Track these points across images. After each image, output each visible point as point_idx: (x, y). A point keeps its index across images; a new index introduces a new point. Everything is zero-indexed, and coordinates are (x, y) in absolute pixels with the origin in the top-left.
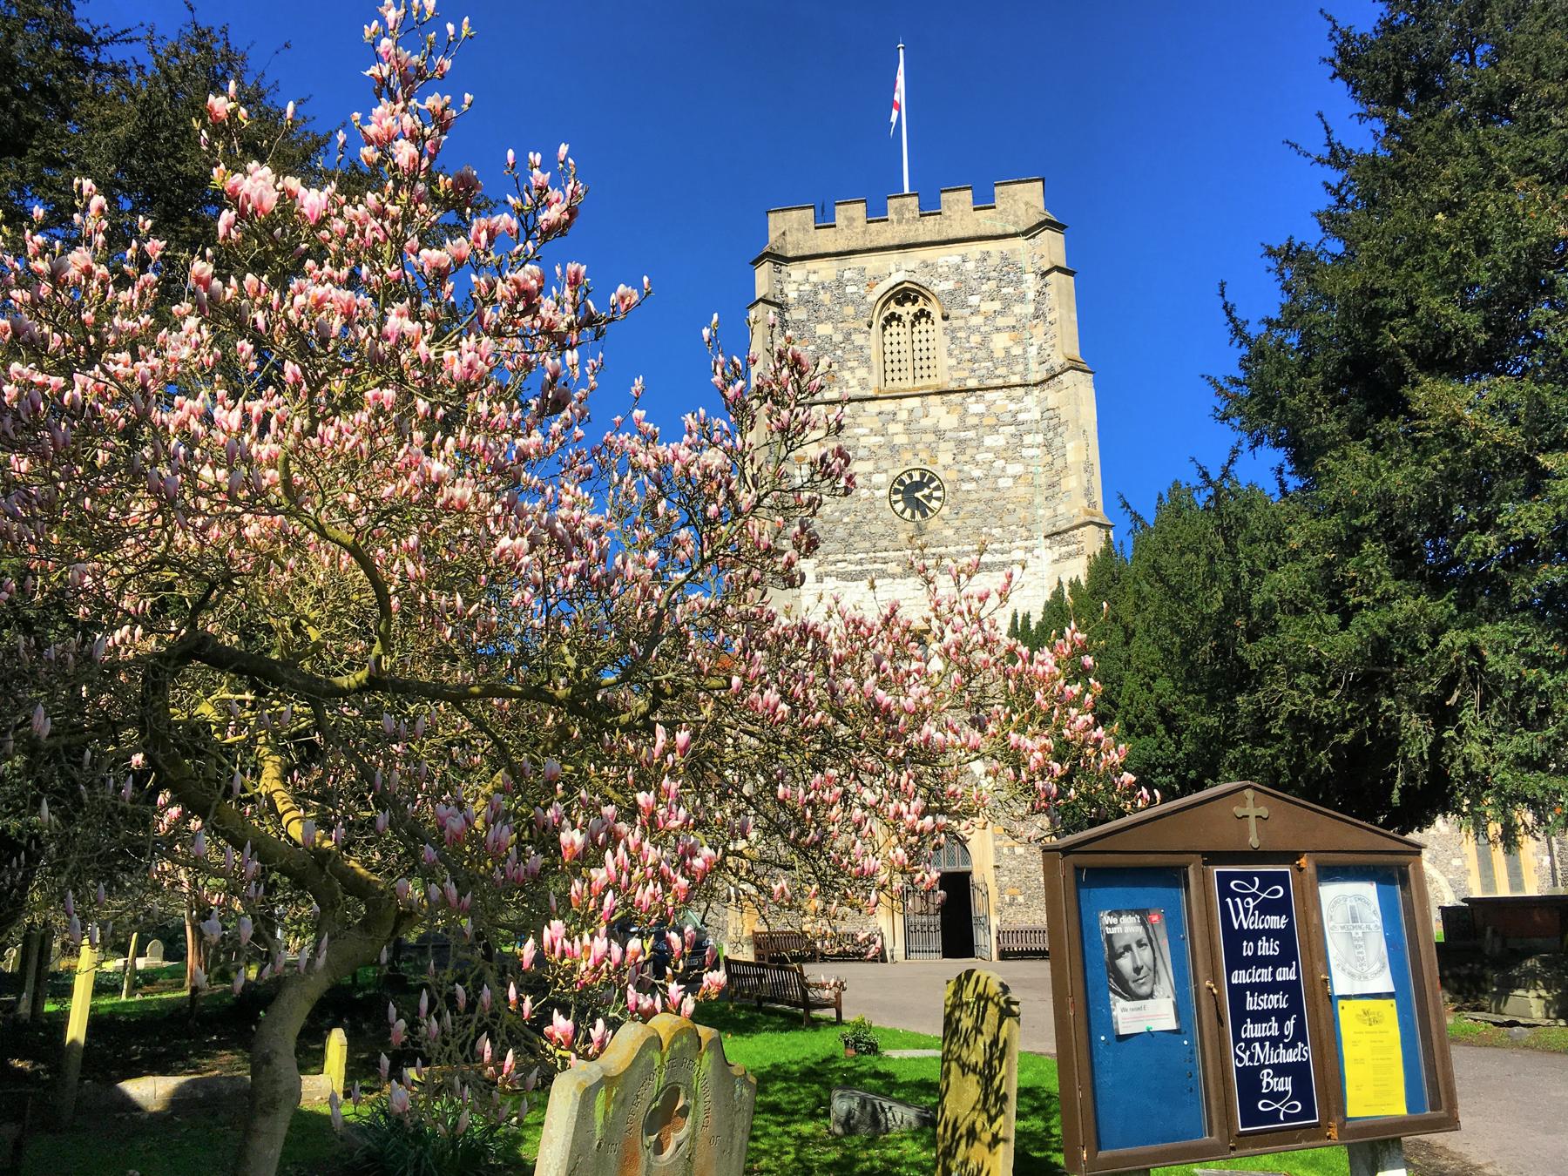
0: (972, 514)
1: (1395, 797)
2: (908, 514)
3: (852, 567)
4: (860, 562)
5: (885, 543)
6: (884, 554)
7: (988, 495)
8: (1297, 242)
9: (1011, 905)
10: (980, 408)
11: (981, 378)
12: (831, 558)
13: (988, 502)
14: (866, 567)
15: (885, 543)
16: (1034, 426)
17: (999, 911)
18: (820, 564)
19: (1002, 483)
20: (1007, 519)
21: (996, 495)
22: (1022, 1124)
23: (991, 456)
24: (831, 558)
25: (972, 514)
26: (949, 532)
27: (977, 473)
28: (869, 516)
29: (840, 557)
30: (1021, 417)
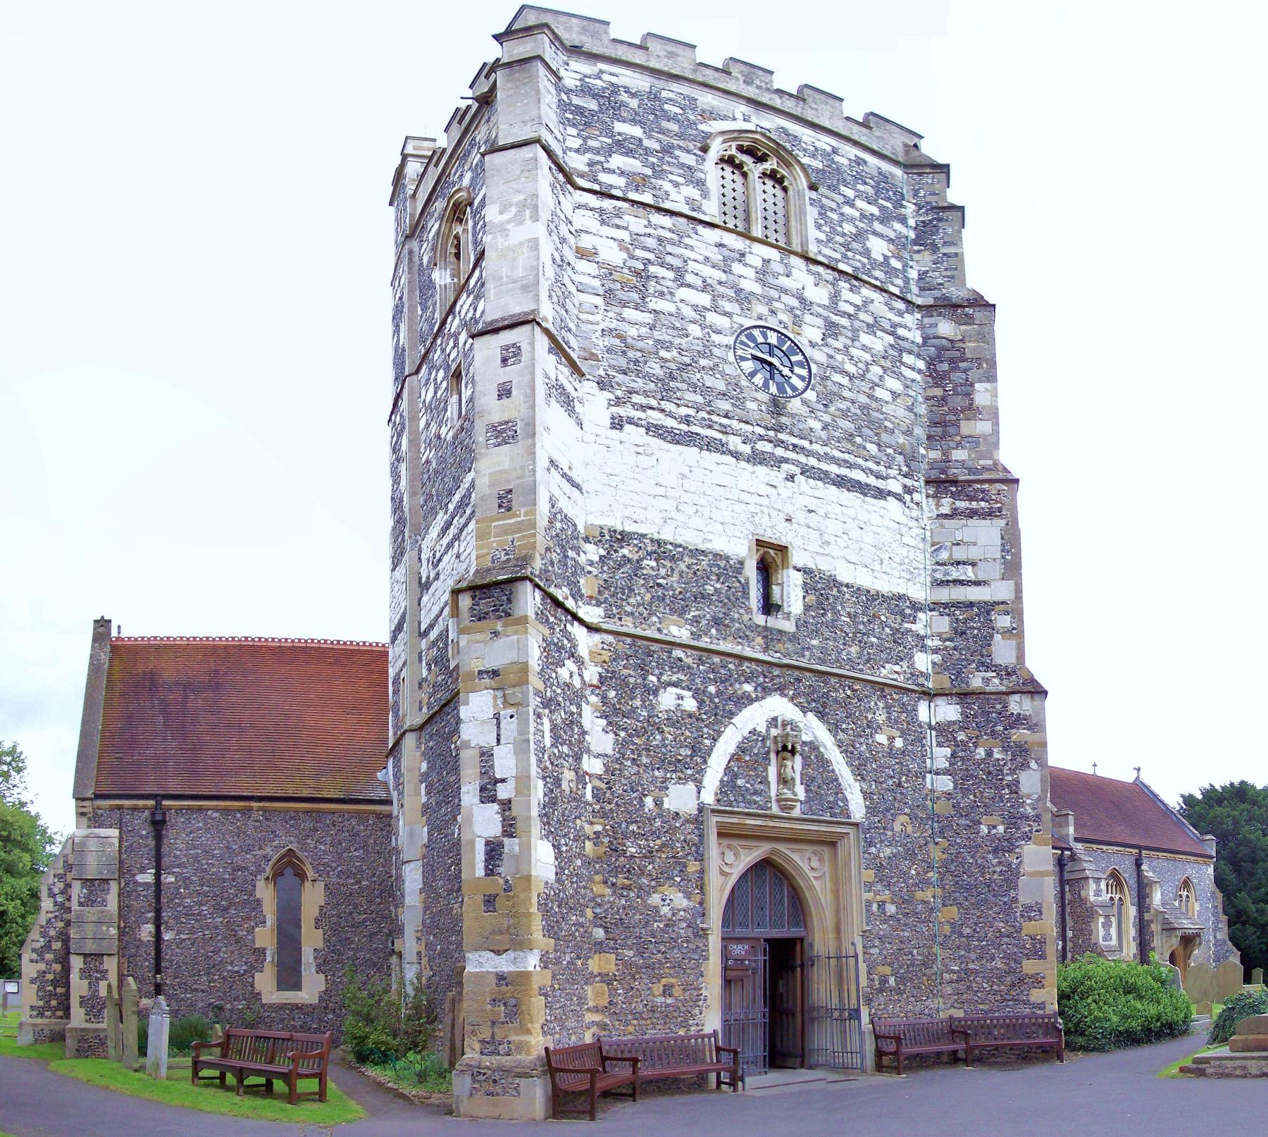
0: (845, 414)
1: (857, 807)
2: (759, 379)
3: (670, 423)
4: (687, 420)
5: (725, 405)
6: (725, 421)
7: (863, 399)
8: (18, 750)
9: (881, 990)
10: (857, 300)
11: (856, 269)
12: (637, 399)
13: (864, 408)
14: (695, 429)
15: (725, 405)
16: (916, 349)
17: (869, 1001)
18: (618, 402)
19: (879, 393)
20: (885, 437)
21: (874, 405)
22: (172, 1060)
23: (868, 357)
24: (637, 399)
25: (845, 414)
26: (817, 426)
27: (850, 368)
28: (703, 362)
29: (654, 403)
30: (901, 331)
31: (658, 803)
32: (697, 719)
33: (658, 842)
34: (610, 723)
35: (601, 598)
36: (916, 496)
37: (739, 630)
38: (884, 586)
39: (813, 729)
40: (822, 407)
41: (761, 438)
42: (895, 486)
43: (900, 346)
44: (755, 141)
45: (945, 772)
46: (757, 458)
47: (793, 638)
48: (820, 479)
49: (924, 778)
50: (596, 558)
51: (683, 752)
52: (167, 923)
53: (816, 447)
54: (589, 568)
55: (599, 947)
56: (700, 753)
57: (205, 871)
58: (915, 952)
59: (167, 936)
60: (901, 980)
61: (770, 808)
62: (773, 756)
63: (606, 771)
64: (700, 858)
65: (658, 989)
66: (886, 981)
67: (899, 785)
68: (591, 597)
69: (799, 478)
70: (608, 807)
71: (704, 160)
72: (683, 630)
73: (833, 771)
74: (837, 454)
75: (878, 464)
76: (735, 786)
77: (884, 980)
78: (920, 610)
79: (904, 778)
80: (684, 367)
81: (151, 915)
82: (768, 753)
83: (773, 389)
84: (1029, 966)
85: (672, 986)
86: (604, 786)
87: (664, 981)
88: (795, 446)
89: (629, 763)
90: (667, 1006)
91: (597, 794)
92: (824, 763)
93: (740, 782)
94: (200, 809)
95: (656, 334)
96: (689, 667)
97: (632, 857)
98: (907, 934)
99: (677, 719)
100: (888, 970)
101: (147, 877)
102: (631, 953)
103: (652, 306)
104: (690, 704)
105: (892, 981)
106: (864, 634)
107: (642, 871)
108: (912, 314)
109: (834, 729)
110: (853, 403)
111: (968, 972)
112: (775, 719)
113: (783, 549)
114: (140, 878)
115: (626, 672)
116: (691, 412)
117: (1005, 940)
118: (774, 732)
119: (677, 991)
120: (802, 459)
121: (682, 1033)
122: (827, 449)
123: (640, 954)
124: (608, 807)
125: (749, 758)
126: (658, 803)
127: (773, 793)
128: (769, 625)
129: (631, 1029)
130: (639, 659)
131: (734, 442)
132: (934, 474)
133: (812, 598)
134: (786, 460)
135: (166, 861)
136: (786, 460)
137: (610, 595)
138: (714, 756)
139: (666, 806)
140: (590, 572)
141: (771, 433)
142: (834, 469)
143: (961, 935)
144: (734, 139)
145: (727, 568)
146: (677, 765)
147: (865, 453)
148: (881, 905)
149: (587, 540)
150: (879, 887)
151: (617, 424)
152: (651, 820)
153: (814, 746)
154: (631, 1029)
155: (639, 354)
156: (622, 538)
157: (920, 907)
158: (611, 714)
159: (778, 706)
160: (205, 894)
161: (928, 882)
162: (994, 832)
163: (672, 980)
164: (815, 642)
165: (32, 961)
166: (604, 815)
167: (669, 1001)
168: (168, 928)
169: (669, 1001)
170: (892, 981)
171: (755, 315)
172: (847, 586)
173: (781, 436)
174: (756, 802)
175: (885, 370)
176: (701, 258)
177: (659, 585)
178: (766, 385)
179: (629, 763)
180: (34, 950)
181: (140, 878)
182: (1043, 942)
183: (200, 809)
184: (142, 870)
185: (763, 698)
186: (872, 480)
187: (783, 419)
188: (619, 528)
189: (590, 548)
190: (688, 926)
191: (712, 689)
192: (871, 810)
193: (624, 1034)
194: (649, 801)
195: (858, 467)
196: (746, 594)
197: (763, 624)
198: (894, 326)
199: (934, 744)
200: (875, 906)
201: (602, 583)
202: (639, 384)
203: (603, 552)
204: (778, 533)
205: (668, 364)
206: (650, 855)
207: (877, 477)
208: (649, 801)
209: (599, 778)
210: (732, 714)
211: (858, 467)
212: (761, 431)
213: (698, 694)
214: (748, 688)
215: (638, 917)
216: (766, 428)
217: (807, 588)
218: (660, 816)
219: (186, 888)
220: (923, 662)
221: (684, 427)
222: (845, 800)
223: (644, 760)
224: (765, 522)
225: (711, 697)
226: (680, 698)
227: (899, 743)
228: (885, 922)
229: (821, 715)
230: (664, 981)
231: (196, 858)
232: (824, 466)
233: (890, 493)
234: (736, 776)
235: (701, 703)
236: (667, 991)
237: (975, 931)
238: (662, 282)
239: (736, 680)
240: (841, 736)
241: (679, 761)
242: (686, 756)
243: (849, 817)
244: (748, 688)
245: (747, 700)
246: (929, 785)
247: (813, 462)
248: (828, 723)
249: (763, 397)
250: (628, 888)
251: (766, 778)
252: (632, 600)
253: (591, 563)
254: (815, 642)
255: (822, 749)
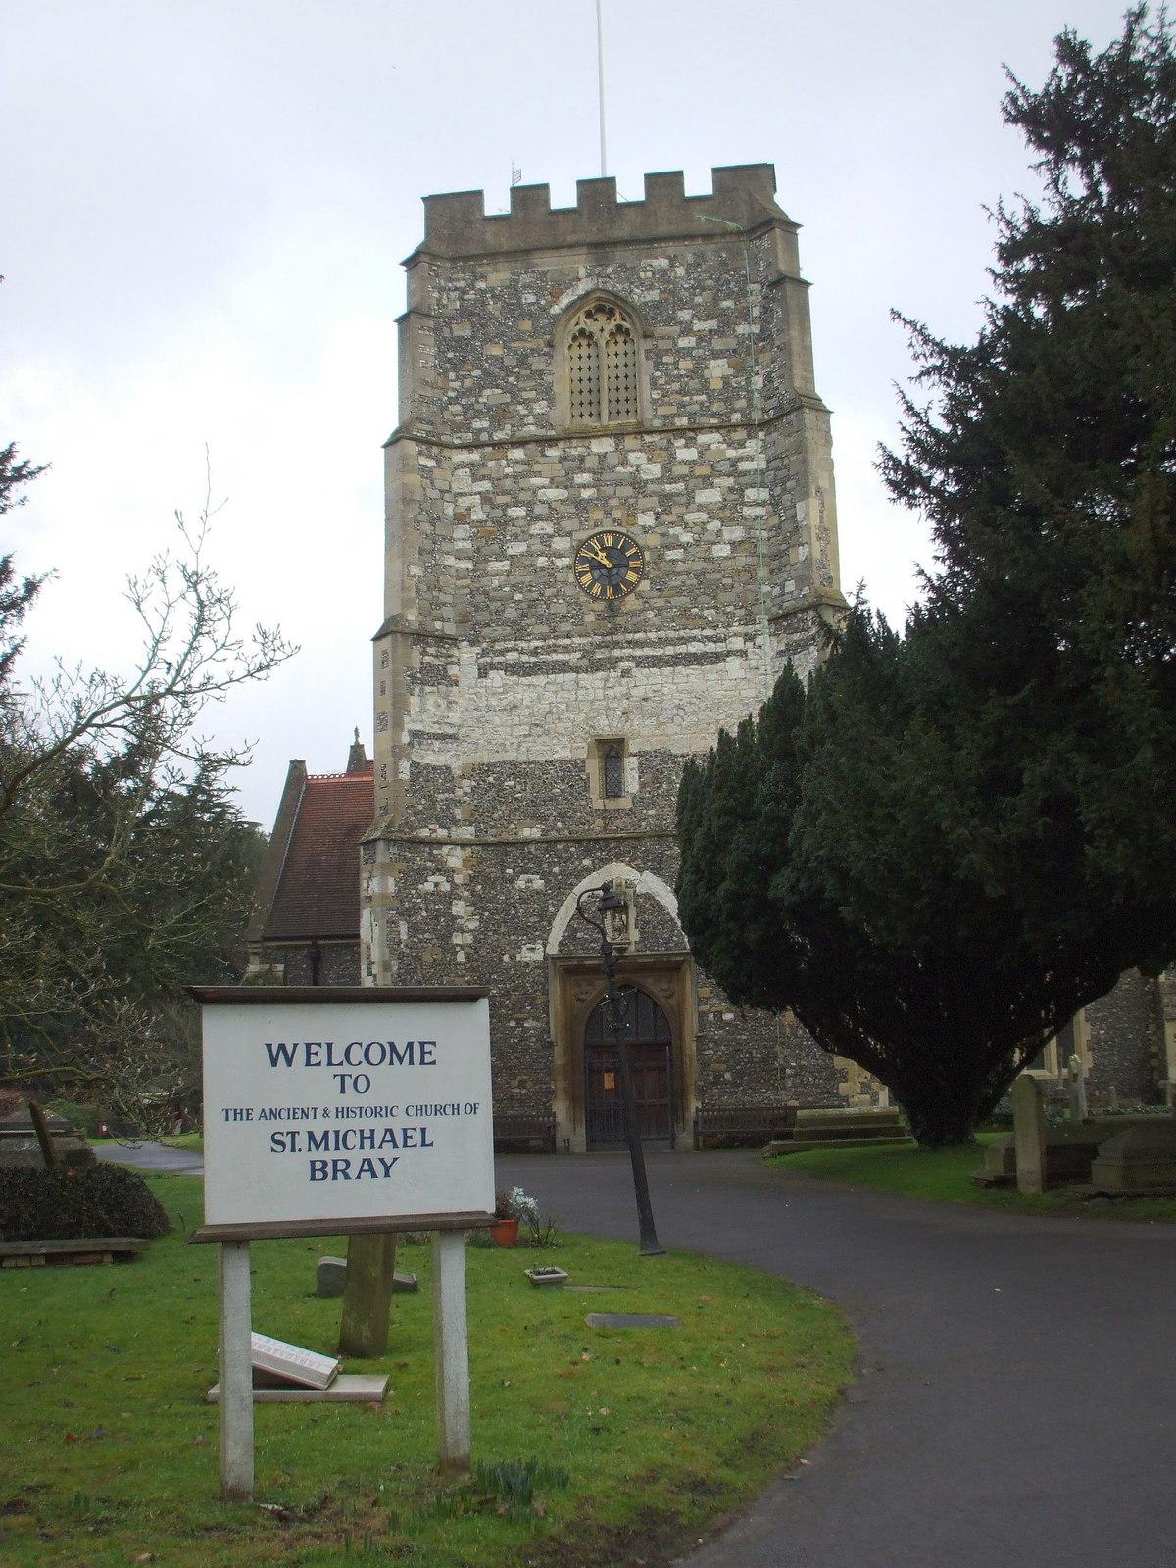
4: (535, 652)
7: (699, 566)
9: (716, 1083)
12: (498, 646)
15: (566, 627)
18: (484, 653)
20: (723, 597)
21: (710, 566)
24: (498, 646)
30: (744, 466)
31: (512, 958)
32: (544, 895)
33: (513, 984)
34: (477, 908)
35: (473, 819)
36: (759, 640)
40: (655, 593)
42: (737, 643)
43: (743, 480)
44: (598, 299)
46: (595, 666)
47: (631, 813)
48: (654, 666)
51: (532, 920)
53: (652, 636)
60: (738, 1075)
64: (546, 993)
69: (636, 672)
71: (551, 357)
72: (535, 830)
74: (672, 634)
77: (719, 1076)
86: (472, 951)
88: (629, 642)
89: (491, 933)
91: (468, 957)
93: (579, 935)
95: (513, 580)
97: (494, 996)
100: (723, 1067)
104: (538, 883)
105: (728, 1076)
108: (756, 437)
110: (688, 574)
116: (539, 643)
119: (529, 1084)
122: (662, 634)
126: (512, 958)
130: (496, 852)
131: (573, 658)
132: (775, 610)
133: (647, 777)
134: (621, 659)
136: (621, 659)
138: (557, 919)
139: (518, 959)
141: (608, 638)
142: (670, 650)
144: (579, 309)
145: (572, 770)
146: (526, 930)
149: (463, 777)
151: (483, 672)
158: (477, 902)
164: (650, 813)
166: (474, 970)
170: (728, 1076)
171: (592, 523)
173: (615, 638)
175: (722, 520)
176: (546, 482)
177: (516, 799)
179: (491, 933)
186: (711, 647)
189: (466, 783)
191: (556, 870)
195: (694, 639)
196: (587, 788)
198: (734, 462)
200: (711, 1016)
202: (500, 631)
208: (506, 958)
209: (470, 946)
211: (694, 639)
214: (587, 863)
216: (602, 635)
221: (533, 659)
223: (502, 930)
224: (603, 722)
225: (555, 876)
226: (530, 881)
228: (721, 1028)
229: (656, 871)
234: (576, 931)
242: (536, 922)
244: (587, 863)
247: (648, 651)
252: (495, 816)
253: (466, 794)
255: (657, 898)
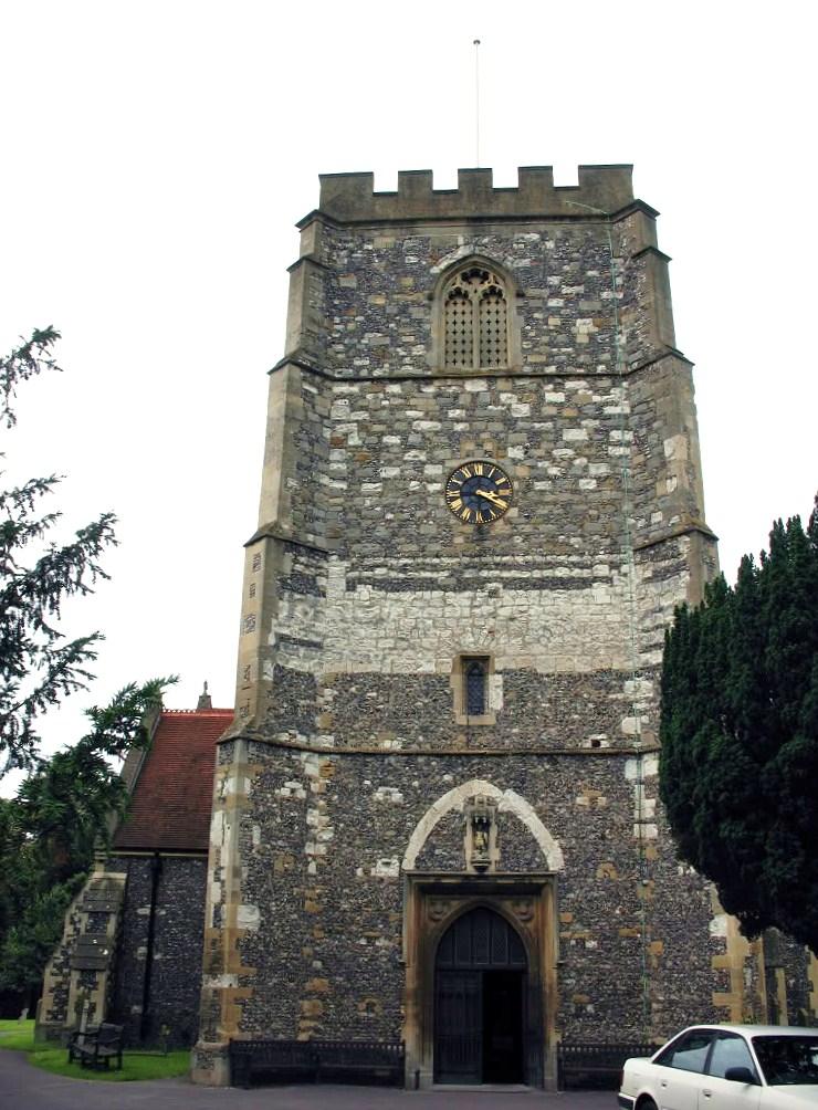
0: (547, 519)
4: (404, 569)
5: (436, 547)
6: (436, 561)
7: (566, 497)
9: (577, 1016)
12: (368, 562)
13: (566, 505)
15: (436, 547)
18: (353, 568)
20: (589, 526)
24: (368, 562)
28: (419, 514)
31: (366, 872)
36: (624, 568)
37: (443, 732)
38: (581, 666)
39: (512, 801)
40: (523, 520)
41: (467, 567)
45: (652, 821)
46: (462, 586)
49: (631, 828)
50: (331, 699)
52: (157, 946)
53: (520, 559)
54: (326, 707)
55: (317, 974)
56: (404, 833)
57: (189, 907)
58: (618, 982)
59: (157, 957)
60: (601, 1007)
61: (465, 869)
62: (469, 830)
63: (328, 853)
64: (399, 910)
65: (362, 1006)
66: (582, 1008)
67: (603, 837)
68: (325, 729)
70: (327, 877)
72: (395, 742)
73: (531, 834)
74: (539, 559)
75: (582, 554)
76: (433, 855)
78: (627, 678)
79: (607, 831)
80: (403, 524)
81: (145, 940)
82: (465, 826)
83: (479, 517)
84: (718, 999)
85: (374, 1005)
86: (325, 863)
87: (367, 1001)
89: (345, 845)
90: (371, 1019)
91: (320, 868)
92: (521, 828)
93: (437, 852)
94: (187, 859)
96: (396, 770)
98: (608, 967)
99: (385, 810)
100: (585, 998)
101: (146, 911)
102: (341, 979)
103: (383, 475)
104: (397, 797)
106: (565, 714)
107: (353, 921)
109: (533, 799)
111: (671, 1002)
112: (472, 799)
113: (486, 659)
114: (141, 911)
115: (346, 781)
117: (698, 972)
118: (470, 808)
120: (505, 574)
121: (381, 1040)
122: (529, 558)
123: (349, 980)
124: (327, 877)
125: (446, 832)
126: (366, 872)
127: (468, 858)
128: (471, 723)
129: (339, 1034)
133: (512, 695)
135: (160, 898)
136: (488, 580)
137: (338, 725)
138: (415, 834)
139: (373, 874)
140: (325, 710)
143: (665, 968)
145: (434, 685)
146: (382, 843)
147: (568, 548)
148: (581, 942)
150: (578, 926)
151: (351, 586)
152: (360, 885)
153: (511, 815)
154: (339, 1034)
155: (370, 522)
156: (352, 678)
157: (624, 943)
158: (333, 812)
159: (482, 788)
160: (186, 924)
161: (635, 920)
162: (687, 872)
163: (374, 1001)
164: (515, 731)
165: (52, 974)
166: (325, 883)
167: (372, 1015)
168: (158, 950)
169: (372, 1015)
170: (590, 1008)
171: (464, 454)
172: (548, 676)
173: (484, 559)
174: (451, 866)
177: (378, 710)
178: (473, 516)
179: (345, 845)
180: (55, 966)
181: (141, 911)
182: (728, 976)
183: (187, 859)
184: (142, 906)
185: (461, 784)
187: (487, 544)
188: (349, 672)
190: (389, 960)
191: (416, 783)
192: (571, 861)
193: (330, 1036)
194: (359, 872)
195: (561, 564)
196: (451, 704)
197: (465, 723)
199: (643, 796)
201: (334, 717)
203: (336, 693)
204: (472, 644)
205: (392, 525)
206: (358, 909)
207: (582, 568)
208: (359, 872)
209: (323, 857)
210: (432, 800)
211: (561, 564)
212: (466, 560)
213: (403, 789)
215: (348, 953)
216: (471, 556)
217: (506, 688)
218: (368, 881)
219: (173, 919)
220: (630, 725)
221: (401, 576)
222: (543, 857)
223: (358, 842)
225: (415, 790)
227: (602, 801)
228: (584, 956)
229: (519, 790)
230: (367, 1001)
231: (183, 897)
232: (526, 575)
233: (595, 579)
234: (434, 847)
235: (406, 795)
236: (370, 1008)
237: (675, 963)
238: (391, 450)
239: (437, 773)
240: (540, 804)
241: (385, 840)
243: (547, 870)
245: (442, 789)
246: (636, 834)
247: (514, 574)
248: (527, 795)
249: (469, 529)
250: (341, 933)
251: (462, 846)
252: (356, 726)
253: (327, 703)
254: (515, 731)
